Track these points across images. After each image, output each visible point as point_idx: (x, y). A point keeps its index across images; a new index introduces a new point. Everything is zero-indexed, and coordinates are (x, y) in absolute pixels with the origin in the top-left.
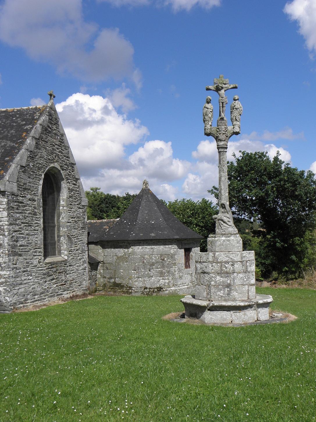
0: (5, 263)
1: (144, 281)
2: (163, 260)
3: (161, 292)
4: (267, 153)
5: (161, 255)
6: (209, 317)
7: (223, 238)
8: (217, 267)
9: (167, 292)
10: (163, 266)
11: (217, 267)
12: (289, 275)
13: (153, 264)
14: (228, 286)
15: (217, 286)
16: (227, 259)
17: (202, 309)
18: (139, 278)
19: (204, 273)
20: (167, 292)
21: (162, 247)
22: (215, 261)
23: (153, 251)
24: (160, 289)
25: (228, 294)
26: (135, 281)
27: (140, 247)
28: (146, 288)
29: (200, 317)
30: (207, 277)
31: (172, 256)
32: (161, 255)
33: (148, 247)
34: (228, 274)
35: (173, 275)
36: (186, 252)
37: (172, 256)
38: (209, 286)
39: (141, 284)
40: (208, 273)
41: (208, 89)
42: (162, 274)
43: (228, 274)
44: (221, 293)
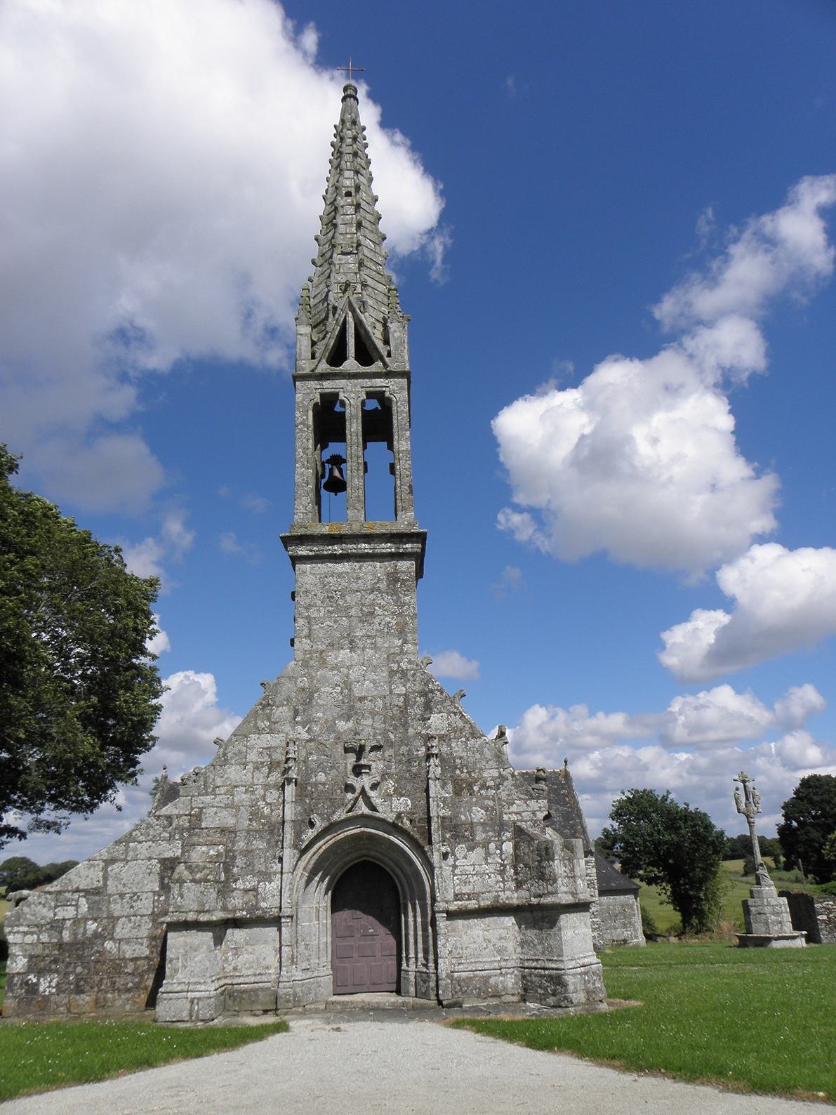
0: (597, 911)
1: (612, 933)
2: (625, 910)
3: (627, 945)
5: (623, 906)
6: (776, 945)
7: (767, 888)
8: (770, 909)
9: (632, 944)
10: (625, 918)
11: (770, 909)
12: (29, 786)
13: (616, 916)
14: (780, 922)
15: (772, 923)
16: (775, 903)
17: (769, 940)
18: (607, 930)
19: (761, 914)
20: (632, 944)
21: (622, 897)
22: (769, 905)
23: (616, 902)
24: (625, 941)
25: (781, 929)
26: (605, 933)
27: (606, 898)
28: (614, 941)
29: (767, 946)
30: (763, 917)
31: (631, 906)
32: (623, 906)
33: (612, 897)
34: (778, 914)
37: (631, 906)
38: (767, 924)
39: (609, 937)
40: (765, 914)
41: (735, 780)
42: (624, 926)
43: (778, 914)
44: (776, 928)
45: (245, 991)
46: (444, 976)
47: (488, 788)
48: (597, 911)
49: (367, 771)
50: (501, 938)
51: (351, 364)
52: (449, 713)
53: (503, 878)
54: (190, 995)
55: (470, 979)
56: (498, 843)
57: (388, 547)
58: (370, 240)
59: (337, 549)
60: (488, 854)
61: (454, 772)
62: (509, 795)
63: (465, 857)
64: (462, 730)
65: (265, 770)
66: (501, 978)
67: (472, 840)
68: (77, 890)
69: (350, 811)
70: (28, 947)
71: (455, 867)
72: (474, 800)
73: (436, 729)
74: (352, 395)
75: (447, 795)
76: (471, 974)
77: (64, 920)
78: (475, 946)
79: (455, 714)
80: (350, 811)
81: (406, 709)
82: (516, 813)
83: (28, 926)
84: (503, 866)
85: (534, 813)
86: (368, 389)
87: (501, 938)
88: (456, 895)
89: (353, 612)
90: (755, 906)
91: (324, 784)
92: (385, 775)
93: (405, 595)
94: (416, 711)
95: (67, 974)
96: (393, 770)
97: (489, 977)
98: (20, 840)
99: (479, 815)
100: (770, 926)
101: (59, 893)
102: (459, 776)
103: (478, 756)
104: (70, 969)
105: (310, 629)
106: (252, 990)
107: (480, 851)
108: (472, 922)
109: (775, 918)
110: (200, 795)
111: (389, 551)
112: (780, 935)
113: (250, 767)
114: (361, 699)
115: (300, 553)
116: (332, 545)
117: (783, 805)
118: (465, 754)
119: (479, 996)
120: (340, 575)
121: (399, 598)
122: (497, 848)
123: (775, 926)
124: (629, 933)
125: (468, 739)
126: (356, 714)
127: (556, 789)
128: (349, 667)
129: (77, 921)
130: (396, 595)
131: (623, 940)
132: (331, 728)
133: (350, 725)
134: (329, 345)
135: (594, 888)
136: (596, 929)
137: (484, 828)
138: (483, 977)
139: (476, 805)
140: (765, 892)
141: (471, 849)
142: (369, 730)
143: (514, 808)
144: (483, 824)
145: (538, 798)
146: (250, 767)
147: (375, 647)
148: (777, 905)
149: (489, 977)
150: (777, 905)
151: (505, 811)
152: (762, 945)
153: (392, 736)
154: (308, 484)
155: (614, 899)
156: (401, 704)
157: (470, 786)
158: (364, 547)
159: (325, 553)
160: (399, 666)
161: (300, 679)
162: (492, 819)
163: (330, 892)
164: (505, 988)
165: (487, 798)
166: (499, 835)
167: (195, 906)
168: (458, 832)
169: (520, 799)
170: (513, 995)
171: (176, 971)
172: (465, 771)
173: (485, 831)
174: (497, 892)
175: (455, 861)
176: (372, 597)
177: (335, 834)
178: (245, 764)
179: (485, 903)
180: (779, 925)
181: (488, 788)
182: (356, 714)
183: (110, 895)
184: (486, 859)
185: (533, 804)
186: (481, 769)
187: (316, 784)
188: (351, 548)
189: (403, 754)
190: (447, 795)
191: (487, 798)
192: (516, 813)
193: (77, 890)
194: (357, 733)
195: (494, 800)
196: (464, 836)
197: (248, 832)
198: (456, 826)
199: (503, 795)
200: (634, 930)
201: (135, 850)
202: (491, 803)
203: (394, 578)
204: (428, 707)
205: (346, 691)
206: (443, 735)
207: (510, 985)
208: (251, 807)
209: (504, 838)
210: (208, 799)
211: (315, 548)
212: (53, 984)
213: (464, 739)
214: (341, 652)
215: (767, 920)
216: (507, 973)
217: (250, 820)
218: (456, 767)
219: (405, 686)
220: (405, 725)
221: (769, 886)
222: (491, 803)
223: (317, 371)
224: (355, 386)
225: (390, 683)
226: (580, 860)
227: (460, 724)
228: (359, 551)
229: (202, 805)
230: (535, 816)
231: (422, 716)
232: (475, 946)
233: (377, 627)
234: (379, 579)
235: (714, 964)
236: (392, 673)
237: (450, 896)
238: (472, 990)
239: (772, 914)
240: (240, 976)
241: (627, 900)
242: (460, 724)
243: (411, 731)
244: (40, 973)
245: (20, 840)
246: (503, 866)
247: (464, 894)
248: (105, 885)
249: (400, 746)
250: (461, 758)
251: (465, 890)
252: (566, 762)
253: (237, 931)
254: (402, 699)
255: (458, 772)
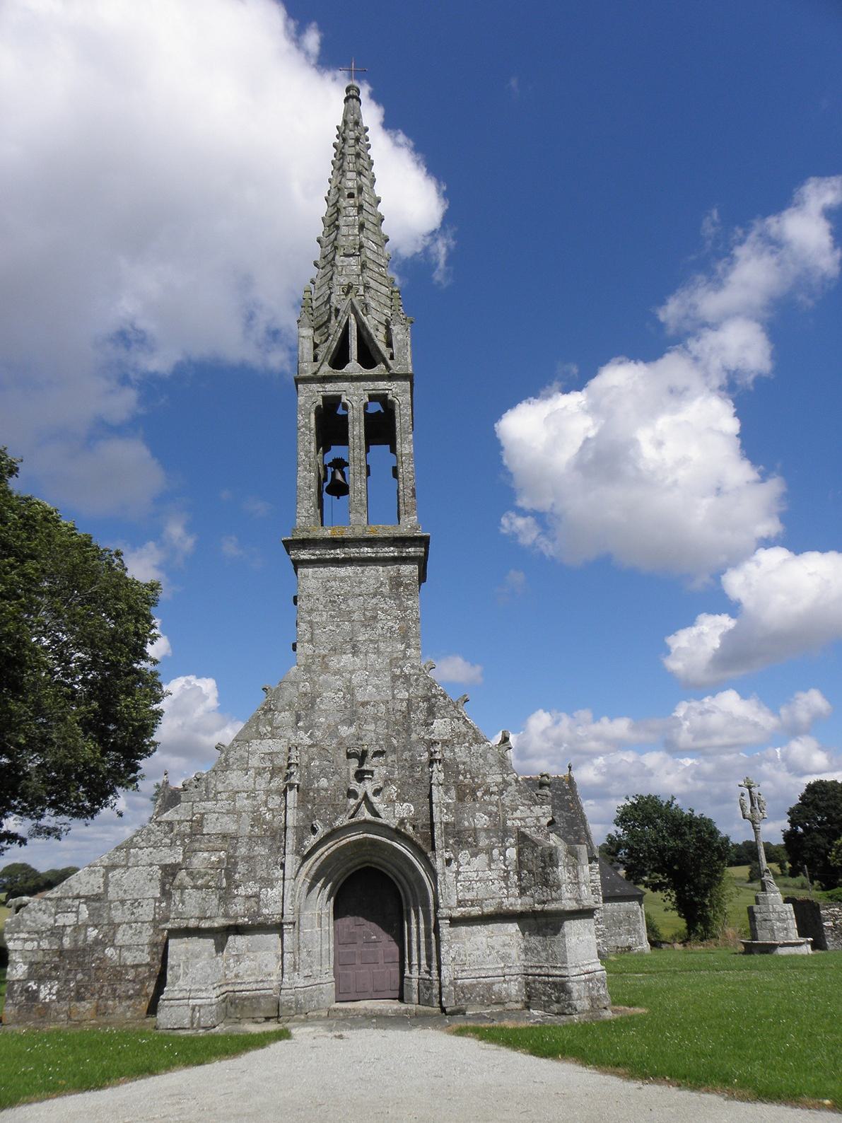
0: (601, 918)
1: (616, 939)
2: (629, 917)
3: (631, 952)
4: (17, 476)
5: (627, 912)
6: (781, 951)
7: (773, 895)
8: (776, 915)
9: (636, 951)
10: (630, 924)
11: (776, 915)
13: (621, 922)
14: (786, 929)
15: (778, 930)
16: (781, 910)
17: (774, 946)
18: (611, 936)
19: (766, 920)
20: (636, 951)
21: (627, 903)
22: (774, 911)
23: (620, 909)
24: (630, 948)
25: (787, 935)
27: (610, 904)
28: (618, 947)
29: (772, 953)
30: (769, 923)
31: (636, 913)
32: (627, 912)
33: (616, 904)
34: (784, 920)
35: (639, 933)
36: (256, 910)
37: (636, 913)
38: (772, 930)
40: (770, 920)
41: (740, 786)
42: (629, 932)
43: (784, 920)
44: (782, 935)
45: (247, 998)
46: (447, 983)
47: (492, 793)
48: (601, 918)
49: (370, 776)
50: (504, 945)
51: (353, 367)
52: (452, 718)
53: (506, 884)
54: (192, 1002)
55: (474, 986)
56: (502, 849)
57: (391, 551)
58: (373, 242)
59: (339, 553)
60: (491, 860)
61: (457, 777)
62: (512, 801)
63: (468, 864)
64: (465, 735)
65: (267, 775)
66: (505, 985)
67: (476, 846)
68: (78, 897)
69: (352, 817)
70: (28, 954)
71: (458, 873)
72: (478, 805)
73: (439, 735)
74: (355, 398)
75: (450, 801)
76: (475, 981)
77: (64, 926)
78: (479, 952)
79: (458, 719)
80: (352, 817)
81: (409, 714)
82: (520, 819)
83: (29, 933)
84: (507, 872)
85: (538, 819)
86: (370, 392)
87: (504, 945)
88: (459, 902)
89: (355, 616)
90: (760, 913)
91: (326, 790)
92: (388, 781)
93: (408, 600)
94: (419, 716)
95: (67, 981)
96: (396, 776)
97: (493, 984)
98: (21, 846)
99: (482, 820)
100: (776, 933)
101: (60, 899)
102: (462, 781)
103: (481, 761)
104: (71, 976)
105: (312, 634)
106: (254, 997)
107: (483, 857)
108: (475, 928)
109: (781, 925)
110: (201, 800)
111: (392, 555)
112: (785, 942)
113: (252, 772)
114: (364, 704)
115: (302, 557)
116: (335, 548)
117: (788, 811)
118: (468, 759)
119: (482, 1003)
120: (342, 580)
121: (402, 602)
122: (500, 854)
123: (781, 932)
124: (634, 939)
125: (471, 745)
126: (359, 719)
127: (560, 795)
128: (352, 672)
129: (77, 928)
130: (399, 599)
131: (627, 947)
132: (333, 733)
133: (353, 730)
134: (332, 348)
135: (599, 894)
136: (600, 935)
137: (487, 834)
138: (487, 984)
139: (479, 811)
140: (770, 898)
141: (474, 855)
142: (372, 735)
143: (518, 814)
144: (487, 830)
145: (542, 804)
146: (252, 772)
147: (378, 652)
148: (782, 912)
149: (493, 984)
150: (782, 912)
151: (509, 817)
152: (767, 952)
153: (395, 741)
154: (310, 488)
155: (619, 905)
156: (403, 709)
157: (474, 792)
158: (367, 551)
159: (328, 557)
160: (402, 671)
161: (302, 684)
162: (495, 825)
163: (333, 898)
164: (508, 995)
165: (491, 803)
166: (503, 841)
167: (197, 913)
168: (461, 838)
169: (524, 805)
170: (517, 1002)
171: (178, 978)
172: (468, 776)
173: (489, 837)
174: (501, 898)
175: (458, 867)
176: (374, 601)
177: (338, 840)
178: (247, 770)
179: (489, 909)
180: (785, 931)
181: (492, 793)
182: (359, 719)
183: (111, 902)
184: (489, 865)
185: (537, 810)
186: (485, 775)
187: (318, 790)
188: (353, 552)
189: (406, 760)
190: (450, 801)
191: (491, 803)
192: (520, 819)
193: (78, 897)
194: (359, 739)
195: (497, 806)
196: (467, 842)
197: (250, 838)
198: (459, 832)
199: (507, 801)
200: (638, 937)
201: (136, 856)
202: (495, 809)
203: (396, 583)
204: (431, 712)
205: (348, 696)
206: (447, 740)
207: (514, 992)
208: (253, 813)
209: (508, 844)
210: (209, 805)
211: (317, 552)
212: (54, 991)
213: (467, 744)
214: (344, 656)
215: (773, 927)
216: (511, 980)
217: (252, 826)
218: (459, 773)
219: (407, 691)
220: (408, 731)
221: (775, 892)
222: (495, 809)
223: (319, 374)
224: (358, 389)
225: (393, 688)
226: (585, 866)
227: (464, 729)
228: (362, 555)
229: (203, 811)
230: (539, 822)
231: (425, 721)
232: (479, 952)
233: (380, 631)
234: (382, 584)
235: (719, 971)
236: (395, 678)
237: (454, 903)
238: (475, 997)
239: (778, 921)
240: (241, 983)
241: (632, 906)
242: (464, 729)
243: (414, 737)
244: (41, 980)
245: (21, 846)
246: (507, 872)
247: (468, 901)
248: (106, 891)
249: (403, 751)
250: (464, 763)
251: (469, 896)
252: (570, 767)
253: (238, 938)
254: (405, 704)
255: (461, 777)
